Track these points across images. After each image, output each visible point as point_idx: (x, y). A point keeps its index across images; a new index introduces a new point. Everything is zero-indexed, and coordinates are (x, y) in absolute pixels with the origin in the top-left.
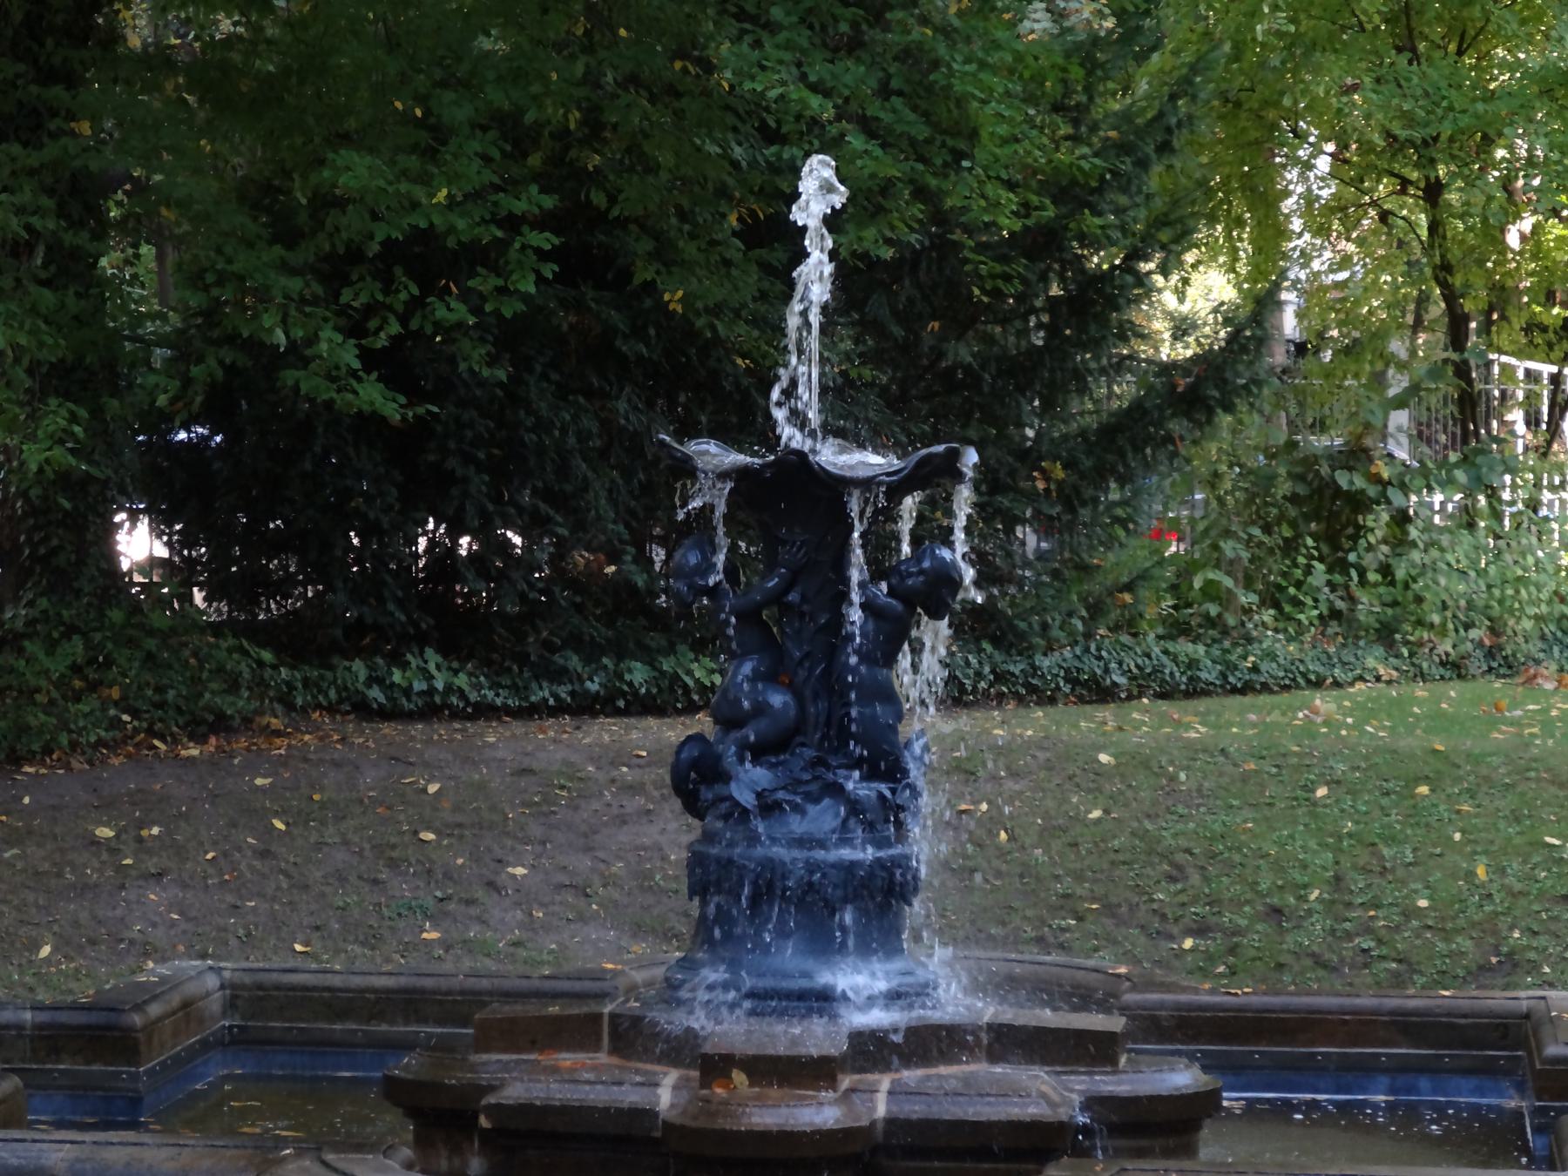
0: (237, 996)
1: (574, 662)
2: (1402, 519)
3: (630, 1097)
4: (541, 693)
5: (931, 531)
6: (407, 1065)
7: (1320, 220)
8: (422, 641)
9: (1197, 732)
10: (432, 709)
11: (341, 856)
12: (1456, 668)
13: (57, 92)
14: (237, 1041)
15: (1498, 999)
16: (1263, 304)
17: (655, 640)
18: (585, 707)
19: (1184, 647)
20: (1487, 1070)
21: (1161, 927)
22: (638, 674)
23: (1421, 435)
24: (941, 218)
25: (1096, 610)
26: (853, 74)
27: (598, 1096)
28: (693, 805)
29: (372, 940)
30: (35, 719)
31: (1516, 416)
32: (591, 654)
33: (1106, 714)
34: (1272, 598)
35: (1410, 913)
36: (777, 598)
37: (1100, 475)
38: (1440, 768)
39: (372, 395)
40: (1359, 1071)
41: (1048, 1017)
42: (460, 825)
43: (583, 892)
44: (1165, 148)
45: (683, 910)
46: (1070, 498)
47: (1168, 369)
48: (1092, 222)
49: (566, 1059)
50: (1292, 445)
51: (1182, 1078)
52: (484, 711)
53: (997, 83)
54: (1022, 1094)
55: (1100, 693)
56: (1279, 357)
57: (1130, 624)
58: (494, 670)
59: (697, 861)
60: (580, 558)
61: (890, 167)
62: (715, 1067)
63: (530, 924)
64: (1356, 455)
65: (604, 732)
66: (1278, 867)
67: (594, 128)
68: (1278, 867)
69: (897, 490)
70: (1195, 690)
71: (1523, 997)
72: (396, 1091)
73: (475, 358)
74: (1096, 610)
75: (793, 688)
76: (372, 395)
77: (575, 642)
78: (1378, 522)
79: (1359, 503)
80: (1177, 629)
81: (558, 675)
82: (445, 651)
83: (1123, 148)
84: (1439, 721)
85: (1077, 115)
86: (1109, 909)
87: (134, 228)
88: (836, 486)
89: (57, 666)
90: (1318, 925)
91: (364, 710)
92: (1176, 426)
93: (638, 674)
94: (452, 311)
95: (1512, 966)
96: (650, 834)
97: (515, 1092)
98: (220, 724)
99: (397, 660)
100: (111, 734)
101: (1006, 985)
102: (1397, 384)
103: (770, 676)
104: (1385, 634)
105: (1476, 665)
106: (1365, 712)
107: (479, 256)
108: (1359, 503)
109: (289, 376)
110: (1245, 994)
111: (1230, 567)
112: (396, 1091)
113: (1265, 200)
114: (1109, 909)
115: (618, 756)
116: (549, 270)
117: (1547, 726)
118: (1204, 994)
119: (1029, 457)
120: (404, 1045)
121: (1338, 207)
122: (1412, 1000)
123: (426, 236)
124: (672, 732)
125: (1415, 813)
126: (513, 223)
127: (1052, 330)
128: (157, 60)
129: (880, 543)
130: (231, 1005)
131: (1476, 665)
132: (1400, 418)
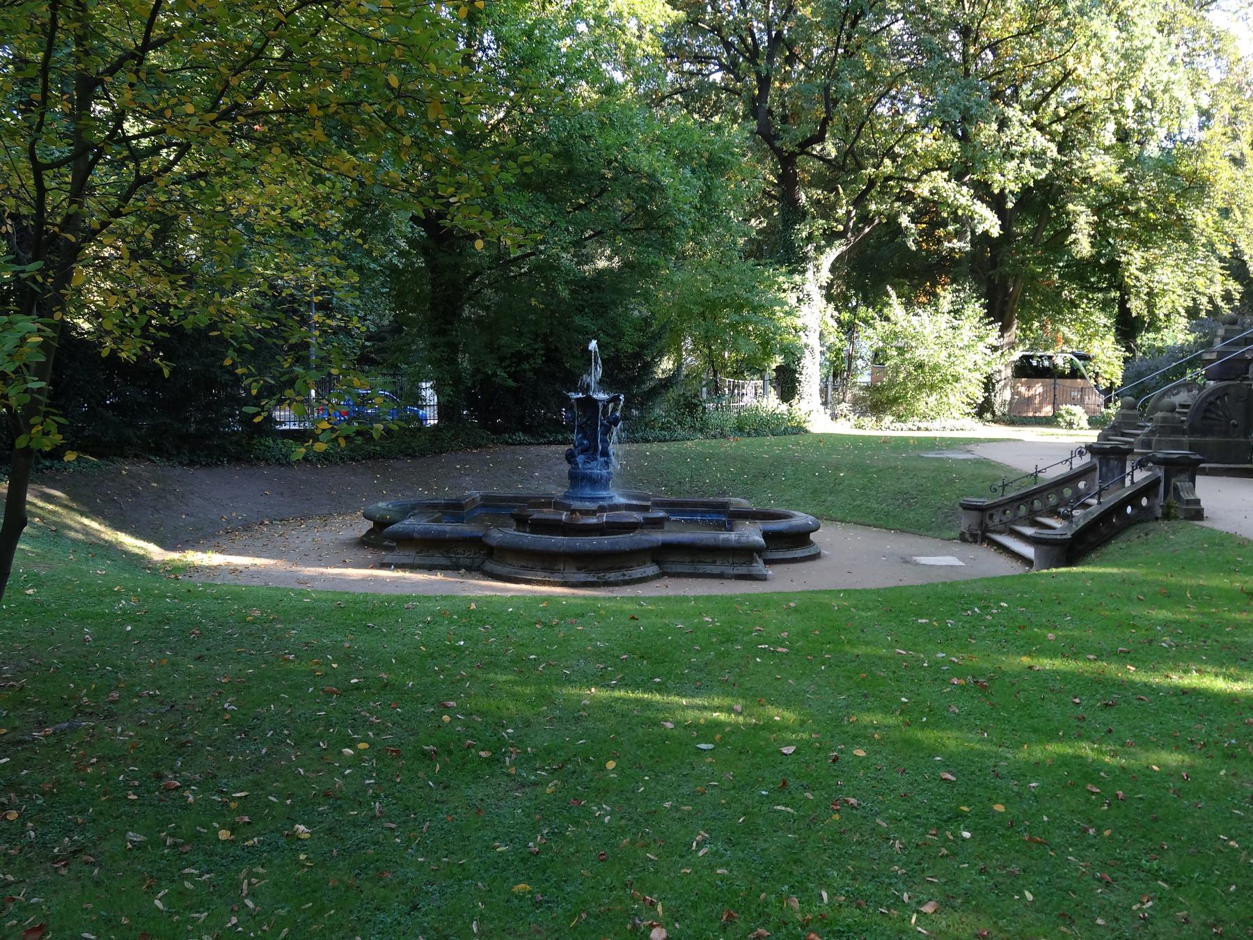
0: (482, 498)
1: (548, 434)
2: (705, 408)
3: (558, 517)
4: (542, 440)
5: (615, 410)
6: (515, 511)
7: (689, 353)
8: (519, 430)
9: (665, 448)
10: (521, 443)
11: (503, 471)
12: (714, 437)
13: (449, 327)
14: (483, 506)
15: (721, 499)
16: (679, 367)
17: (563, 430)
18: (550, 443)
19: (663, 432)
20: (719, 513)
21: (659, 485)
22: (560, 437)
23: (709, 393)
24: (617, 350)
25: (647, 425)
26: (601, 321)
27: (552, 517)
28: (569, 462)
29: (509, 487)
30: (445, 445)
31: (726, 389)
32: (551, 433)
33: (648, 445)
34: (679, 423)
35: (705, 483)
36: (585, 423)
37: (648, 399)
38: (711, 456)
39: (511, 383)
40: (694, 513)
41: (634, 502)
42: (714, 819)
43: (549, 478)
44: (660, 338)
45: (567, 482)
46: (642, 404)
47: (660, 380)
48: (646, 352)
49: (545, 510)
50: (684, 394)
51: (661, 514)
52: (531, 444)
53: (628, 324)
54: (632, 517)
55: (647, 441)
56: (682, 378)
57: (653, 428)
58: (533, 437)
59: (570, 473)
60: (549, 414)
61: (609, 340)
62: (573, 511)
63: (539, 484)
64: (696, 396)
65: (553, 448)
66: (680, 474)
67: (552, 333)
68: (680, 474)
69: (609, 402)
70: (665, 441)
71: (726, 499)
72: (513, 516)
73: (530, 374)
74: (647, 425)
75: (588, 439)
76: (511, 383)
77: (548, 431)
78: (701, 408)
79: (696, 406)
80: (662, 429)
81: (545, 437)
82: (523, 432)
83: (652, 338)
84: (711, 447)
85: (644, 331)
86: (648, 482)
87: (464, 352)
88: (596, 401)
89: (449, 435)
90: (688, 485)
91: (508, 444)
92: (663, 391)
93: (560, 437)
94: (526, 366)
95: (724, 493)
96: (561, 467)
97: (535, 516)
98: (480, 446)
99: (514, 434)
100: (651, 259)
101: (629, 497)
102: (704, 383)
103: (584, 438)
104: (701, 430)
105: (718, 436)
106: (697, 445)
107: (532, 356)
108: (696, 406)
109: (494, 379)
110: (673, 498)
111: (672, 417)
112: (513, 516)
113: (679, 350)
114: (648, 482)
115: (556, 452)
116: (544, 359)
117: (731, 448)
118: (666, 498)
119: (634, 396)
120: (514, 507)
121: (692, 350)
122: (705, 499)
123: (519, 352)
124: (566, 448)
125: (706, 464)
126: (536, 350)
127: (639, 372)
128: (469, 319)
129: (605, 412)
130: (482, 499)
131: (718, 436)
132: (704, 389)
